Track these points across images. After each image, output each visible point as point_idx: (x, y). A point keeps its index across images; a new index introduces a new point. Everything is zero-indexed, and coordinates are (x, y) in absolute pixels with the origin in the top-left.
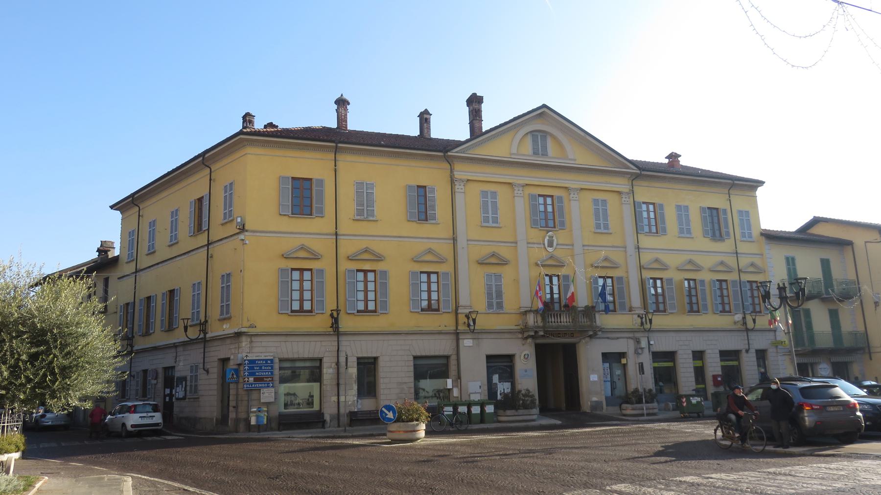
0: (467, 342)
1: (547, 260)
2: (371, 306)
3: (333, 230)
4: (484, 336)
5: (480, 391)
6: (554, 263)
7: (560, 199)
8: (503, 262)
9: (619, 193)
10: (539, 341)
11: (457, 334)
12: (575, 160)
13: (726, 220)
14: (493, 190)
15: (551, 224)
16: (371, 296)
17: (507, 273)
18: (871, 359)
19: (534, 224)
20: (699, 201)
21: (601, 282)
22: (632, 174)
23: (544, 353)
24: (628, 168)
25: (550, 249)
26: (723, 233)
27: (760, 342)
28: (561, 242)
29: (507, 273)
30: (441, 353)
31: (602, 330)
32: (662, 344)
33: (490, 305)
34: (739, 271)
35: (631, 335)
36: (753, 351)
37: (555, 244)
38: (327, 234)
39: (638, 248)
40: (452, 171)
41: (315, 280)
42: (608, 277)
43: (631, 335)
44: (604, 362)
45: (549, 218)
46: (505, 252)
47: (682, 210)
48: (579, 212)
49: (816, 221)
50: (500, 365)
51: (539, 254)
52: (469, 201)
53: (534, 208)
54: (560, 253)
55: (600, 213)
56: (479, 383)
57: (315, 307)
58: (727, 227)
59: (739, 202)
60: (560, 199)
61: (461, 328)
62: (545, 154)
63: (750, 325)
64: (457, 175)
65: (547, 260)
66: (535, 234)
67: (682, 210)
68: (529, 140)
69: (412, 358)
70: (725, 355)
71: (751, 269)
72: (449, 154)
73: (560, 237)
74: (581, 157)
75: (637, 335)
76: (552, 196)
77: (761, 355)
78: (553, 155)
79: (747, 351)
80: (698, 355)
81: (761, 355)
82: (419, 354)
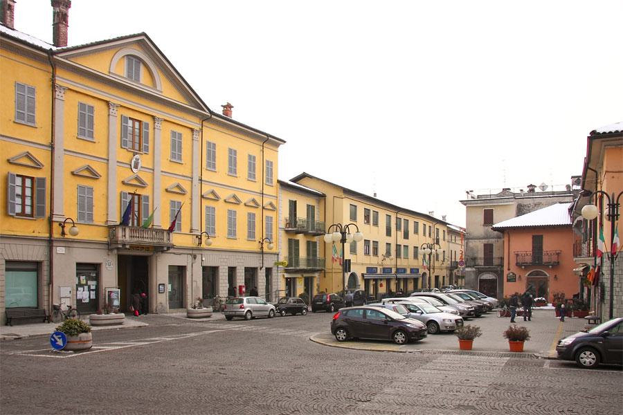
0: (60, 250)
1: (132, 179)
2: (28, 210)
3: (47, 141)
4: (76, 245)
5: (70, 295)
6: (178, 191)
7: (147, 125)
8: (94, 176)
9: (192, 130)
10: (121, 253)
11: (50, 242)
12: (162, 92)
13: (147, 134)
14: (179, 132)
15: (137, 146)
16: (28, 201)
17: (98, 187)
18: (325, 276)
19: (123, 144)
20: (245, 148)
21: (129, 197)
22: (203, 115)
23: (123, 262)
24: (205, 111)
25: (134, 170)
26: (143, 147)
27: (269, 262)
28: (143, 166)
29: (98, 187)
30: (34, 259)
31: (173, 246)
32: (210, 261)
33: (81, 216)
34: (263, 208)
35: (191, 252)
36: (264, 268)
37: (139, 167)
38: (45, 146)
39: (201, 180)
40: (54, 76)
41: (36, 189)
42: (137, 195)
43: (191, 252)
44: (78, 275)
45: (137, 141)
46: (98, 167)
47: (232, 153)
48: (161, 138)
49: (304, 176)
50: (89, 270)
51: (127, 175)
52: (68, 109)
53: (124, 130)
54: (145, 177)
55: (176, 146)
56: (70, 289)
57: (35, 212)
58: (147, 142)
59: (269, 153)
60: (147, 125)
61: (56, 235)
62: (137, 80)
63: (265, 250)
64: (58, 82)
65: (132, 179)
66: (124, 156)
67: (232, 153)
68: (125, 61)
69: (4, 262)
70: (247, 270)
71: (135, 182)
72: (55, 57)
73: (144, 160)
74: (167, 91)
75: (194, 252)
76: (140, 122)
77: (269, 271)
78: (144, 83)
79: (261, 268)
80: (232, 270)
81: (269, 271)
82: (11, 258)
